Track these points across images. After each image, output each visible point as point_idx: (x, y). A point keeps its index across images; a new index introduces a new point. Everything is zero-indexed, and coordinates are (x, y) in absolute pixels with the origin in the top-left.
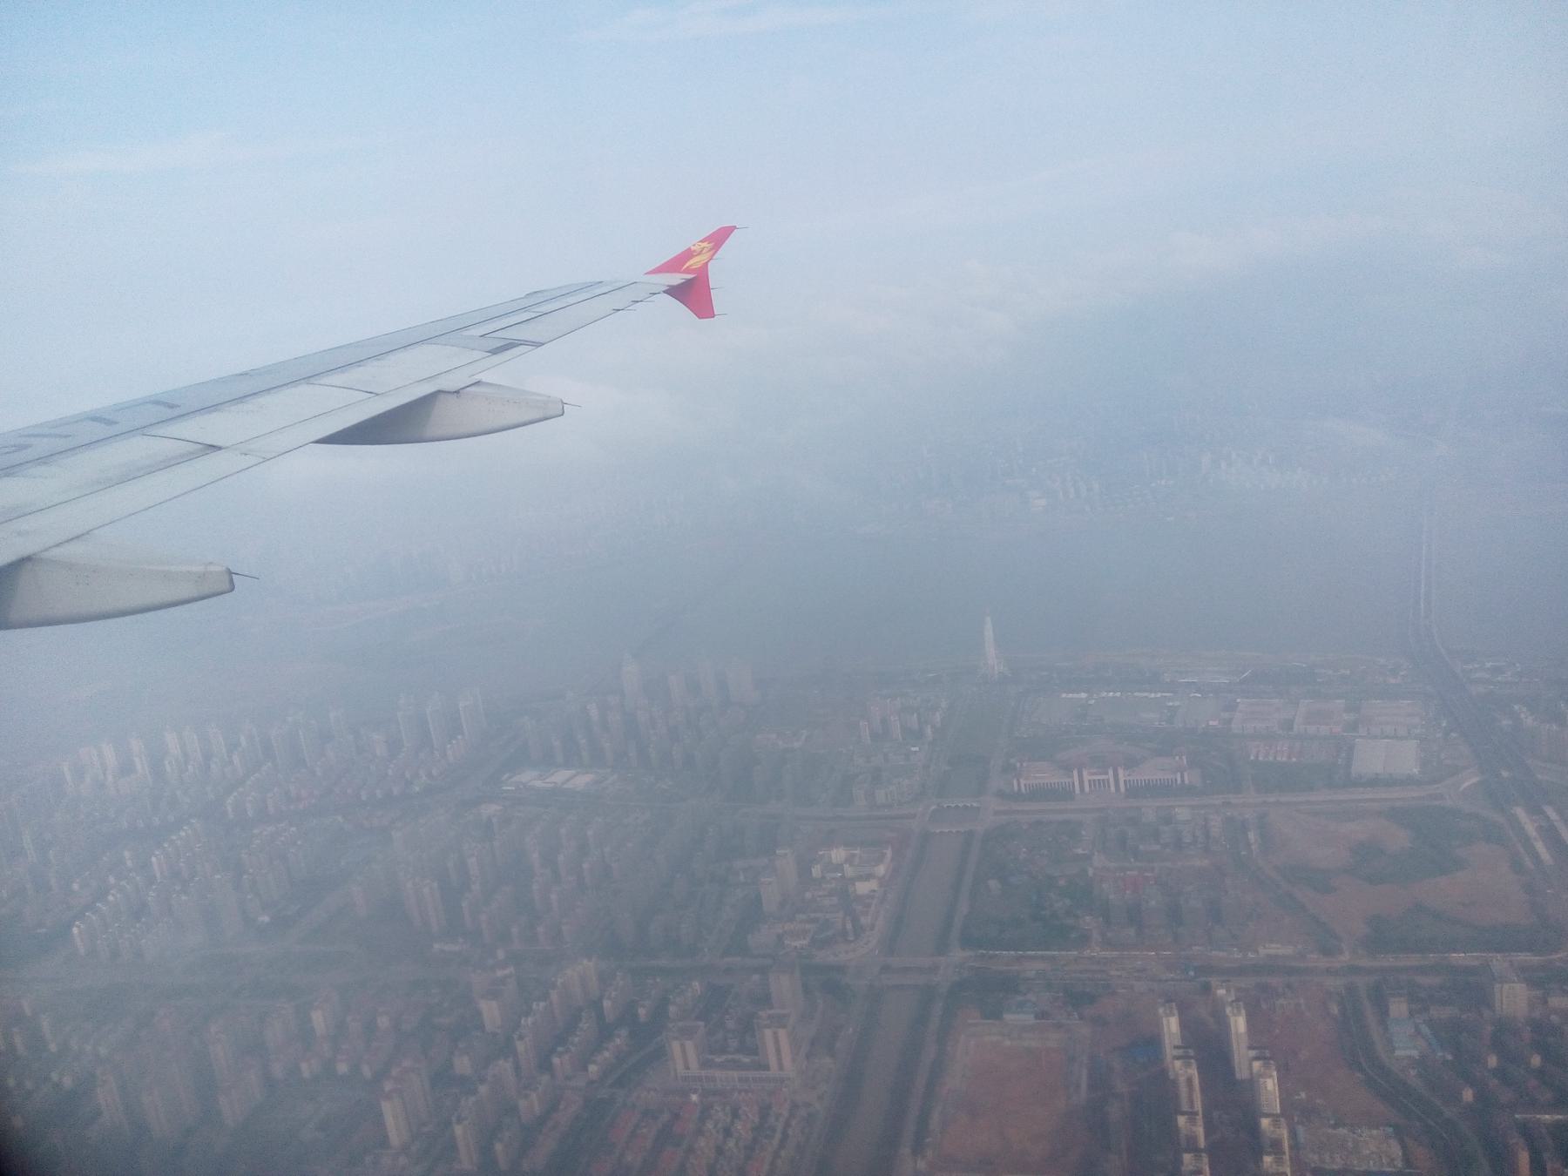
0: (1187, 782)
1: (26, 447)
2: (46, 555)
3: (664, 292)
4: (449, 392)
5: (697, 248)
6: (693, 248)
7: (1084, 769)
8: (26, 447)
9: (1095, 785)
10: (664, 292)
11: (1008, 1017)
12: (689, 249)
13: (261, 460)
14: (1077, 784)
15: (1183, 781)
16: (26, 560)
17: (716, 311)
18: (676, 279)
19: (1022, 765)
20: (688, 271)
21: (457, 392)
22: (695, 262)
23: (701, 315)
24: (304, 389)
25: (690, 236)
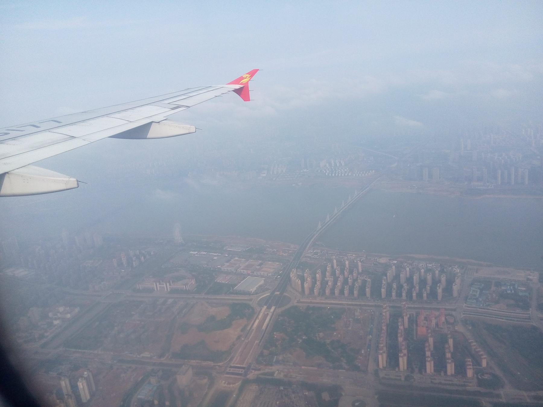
2: (11, 172)
3: (233, 91)
5: (245, 76)
6: (243, 76)
7: (167, 283)
10: (233, 91)
13: (89, 142)
15: (156, 284)
16: (7, 173)
18: (238, 87)
20: (241, 84)
21: (159, 122)
22: (244, 81)
24: (105, 119)
25: (242, 71)
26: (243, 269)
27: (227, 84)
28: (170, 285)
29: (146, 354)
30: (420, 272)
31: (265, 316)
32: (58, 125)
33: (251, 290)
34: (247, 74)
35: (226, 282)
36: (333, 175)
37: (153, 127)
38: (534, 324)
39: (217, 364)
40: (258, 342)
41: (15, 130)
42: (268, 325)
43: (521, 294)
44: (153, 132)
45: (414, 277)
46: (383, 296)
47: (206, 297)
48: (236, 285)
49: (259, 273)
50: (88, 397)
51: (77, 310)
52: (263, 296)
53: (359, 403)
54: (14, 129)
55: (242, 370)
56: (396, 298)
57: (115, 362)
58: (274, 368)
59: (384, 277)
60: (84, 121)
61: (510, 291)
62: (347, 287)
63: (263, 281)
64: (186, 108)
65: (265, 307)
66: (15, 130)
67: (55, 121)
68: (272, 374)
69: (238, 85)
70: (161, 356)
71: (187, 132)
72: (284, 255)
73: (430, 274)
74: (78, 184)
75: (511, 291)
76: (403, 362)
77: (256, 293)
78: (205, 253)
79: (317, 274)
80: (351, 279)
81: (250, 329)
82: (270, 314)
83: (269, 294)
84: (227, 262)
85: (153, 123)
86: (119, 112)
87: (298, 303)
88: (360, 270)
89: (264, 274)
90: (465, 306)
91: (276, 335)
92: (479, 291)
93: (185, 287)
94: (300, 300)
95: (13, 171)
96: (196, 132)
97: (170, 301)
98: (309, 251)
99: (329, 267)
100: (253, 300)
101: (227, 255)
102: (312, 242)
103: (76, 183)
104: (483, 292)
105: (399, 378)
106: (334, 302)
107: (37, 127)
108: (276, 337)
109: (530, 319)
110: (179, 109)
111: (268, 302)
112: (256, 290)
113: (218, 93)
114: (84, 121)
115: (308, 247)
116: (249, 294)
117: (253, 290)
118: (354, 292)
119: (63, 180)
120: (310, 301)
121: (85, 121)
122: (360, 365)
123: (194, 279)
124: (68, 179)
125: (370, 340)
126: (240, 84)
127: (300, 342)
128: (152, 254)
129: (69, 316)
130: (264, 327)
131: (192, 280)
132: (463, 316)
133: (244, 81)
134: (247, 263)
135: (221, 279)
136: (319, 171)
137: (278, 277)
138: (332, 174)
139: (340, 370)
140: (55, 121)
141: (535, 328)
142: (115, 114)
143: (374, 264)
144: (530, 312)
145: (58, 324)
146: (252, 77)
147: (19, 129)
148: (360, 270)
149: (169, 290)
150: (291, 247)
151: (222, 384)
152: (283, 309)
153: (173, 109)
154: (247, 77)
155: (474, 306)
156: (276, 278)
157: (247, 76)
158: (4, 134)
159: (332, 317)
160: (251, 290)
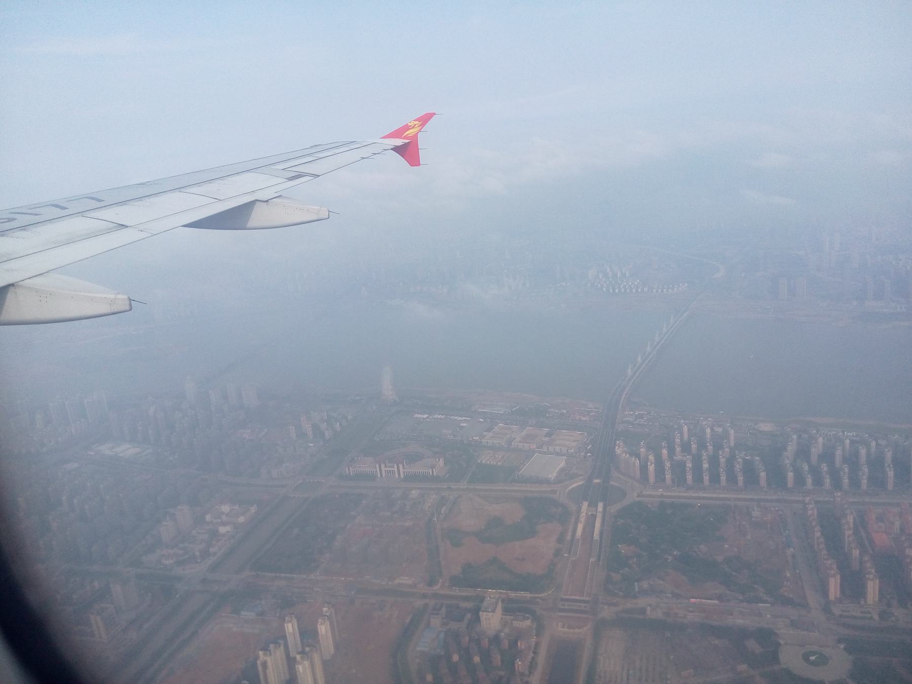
0: (435, 474)
1: (14, 219)
2: (20, 283)
3: (391, 149)
4: (261, 201)
5: (412, 124)
6: (409, 124)
7: (400, 464)
8: (14, 219)
9: (388, 473)
10: (391, 149)
11: (243, 613)
12: (407, 124)
13: (151, 235)
14: (378, 472)
15: (380, 466)
16: (13, 285)
17: (421, 163)
18: (399, 142)
19: (358, 458)
20: (406, 138)
21: (267, 201)
22: (410, 132)
23: (412, 165)
24: (177, 195)
25: (409, 117)
26: (520, 442)
29: (406, 580)
35: (499, 464)
36: (617, 291)
39: (537, 595)
41: (26, 214)
42: (601, 533)
44: (258, 216)
45: (836, 453)
46: (790, 481)
47: (472, 487)
49: (551, 449)
50: (332, 651)
51: (253, 509)
52: (574, 486)
53: (816, 656)
54: (26, 212)
55: (586, 605)
56: (812, 487)
57: (353, 593)
58: (641, 602)
60: (140, 199)
66: (26, 214)
67: (93, 198)
68: (643, 611)
69: (400, 139)
70: (431, 584)
71: (315, 218)
72: (584, 419)
74: (130, 305)
76: (872, 588)
79: (664, 449)
85: (257, 202)
87: (638, 496)
89: (561, 449)
91: (623, 549)
94: (641, 492)
95: (22, 283)
100: (558, 493)
103: (127, 302)
105: (869, 616)
106: (704, 495)
108: (623, 551)
112: (556, 477)
114: (140, 199)
116: (547, 482)
117: (552, 476)
118: (722, 478)
119: (105, 298)
122: (791, 596)
124: (113, 296)
125: (793, 556)
126: (402, 139)
128: (349, 418)
129: (241, 519)
130: (596, 536)
131: (439, 460)
133: (410, 132)
134: (524, 433)
135: (485, 459)
136: (589, 285)
137: (589, 454)
138: (614, 290)
139: (760, 605)
140: (93, 198)
142: (192, 187)
145: (228, 532)
147: (29, 211)
149: (402, 476)
150: (588, 407)
151: (558, 629)
154: (417, 126)
156: (585, 457)
158: (6, 220)
160: (550, 476)
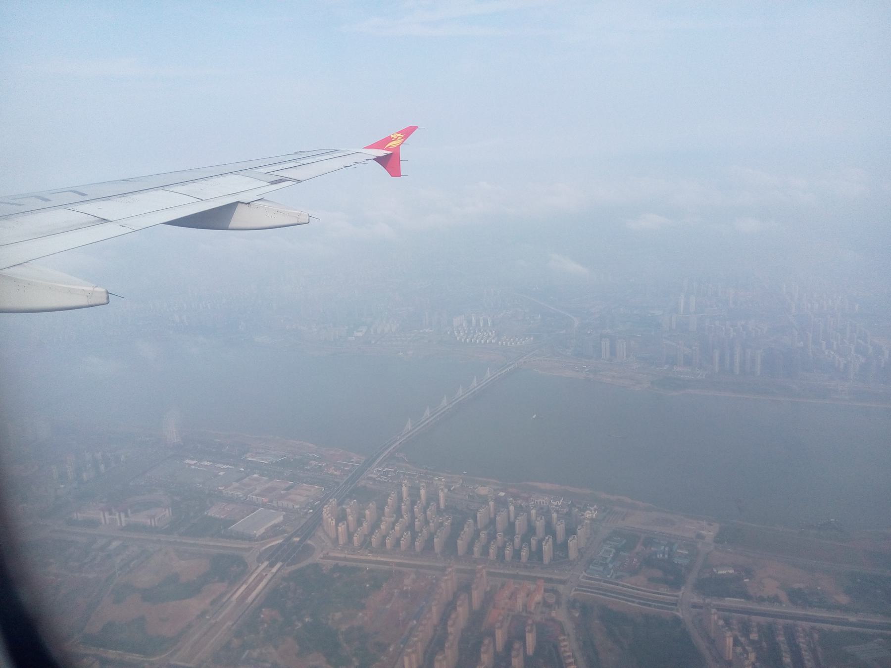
3: (373, 159)
5: (394, 136)
6: (392, 136)
10: (373, 159)
18: (382, 153)
20: (388, 149)
21: (249, 203)
22: (393, 144)
24: (160, 192)
25: (392, 130)
26: (256, 495)
27: (365, 148)
28: (127, 516)
30: (529, 514)
31: (260, 578)
32: (82, 198)
33: (255, 532)
34: (398, 133)
37: (240, 211)
38: (679, 614)
40: (231, 624)
43: (677, 560)
44: (239, 218)
48: (234, 522)
59: (469, 520)
61: (661, 556)
62: (407, 534)
63: (282, 516)
64: (295, 183)
65: (266, 563)
71: (296, 222)
73: (541, 517)
74: (108, 298)
75: (664, 556)
77: (262, 537)
78: (208, 463)
80: (419, 521)
81: (227, 601)
82: (269, 576)
83: (280, 541)
84: (237, 481)
86: (183, 183)
87: (324, 558)
88: (442, 506)
90: (584, 577)
92: (614, 551)
93: (149, 521)
94: (328, 554)
96: (309, 223)
97: (115, 544)
98: (376, 469)
99: (392, 498)
101: (242, 469)
102: (389, 452)
103: (105, 295)
104: (621, 553)
107: (47, 200)
109: (676, 605)
110: (283, 183)
111: (273, 556)
113: (348, 161)
115: (378, 460)
116: (251, 539)
120: (342, 556)
121: (127, 195)
123: (170, 508)
124: (91, 289)
126: (385, 150)
127: (298, 627)
130: (250, 599)
132: (573, 593)
133: (393, 144)
141: (677, 621)
143: (469, 496)
144: (680, 593)
146: (406, 138)
148: (442, 506)
150: (352, 460)
152: (293, 568)
153: (273, 183)
155: (597, 577)
157: (398, 137)
159: (368, 586)
